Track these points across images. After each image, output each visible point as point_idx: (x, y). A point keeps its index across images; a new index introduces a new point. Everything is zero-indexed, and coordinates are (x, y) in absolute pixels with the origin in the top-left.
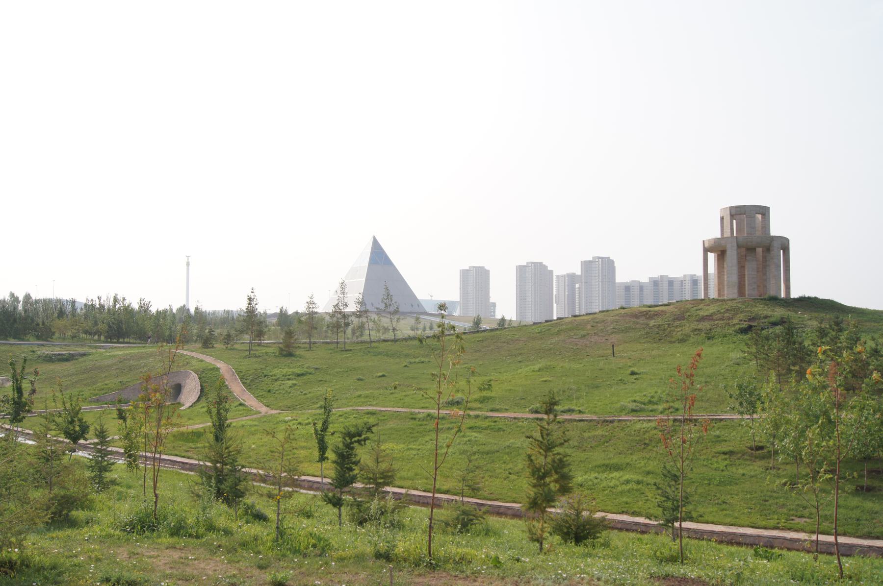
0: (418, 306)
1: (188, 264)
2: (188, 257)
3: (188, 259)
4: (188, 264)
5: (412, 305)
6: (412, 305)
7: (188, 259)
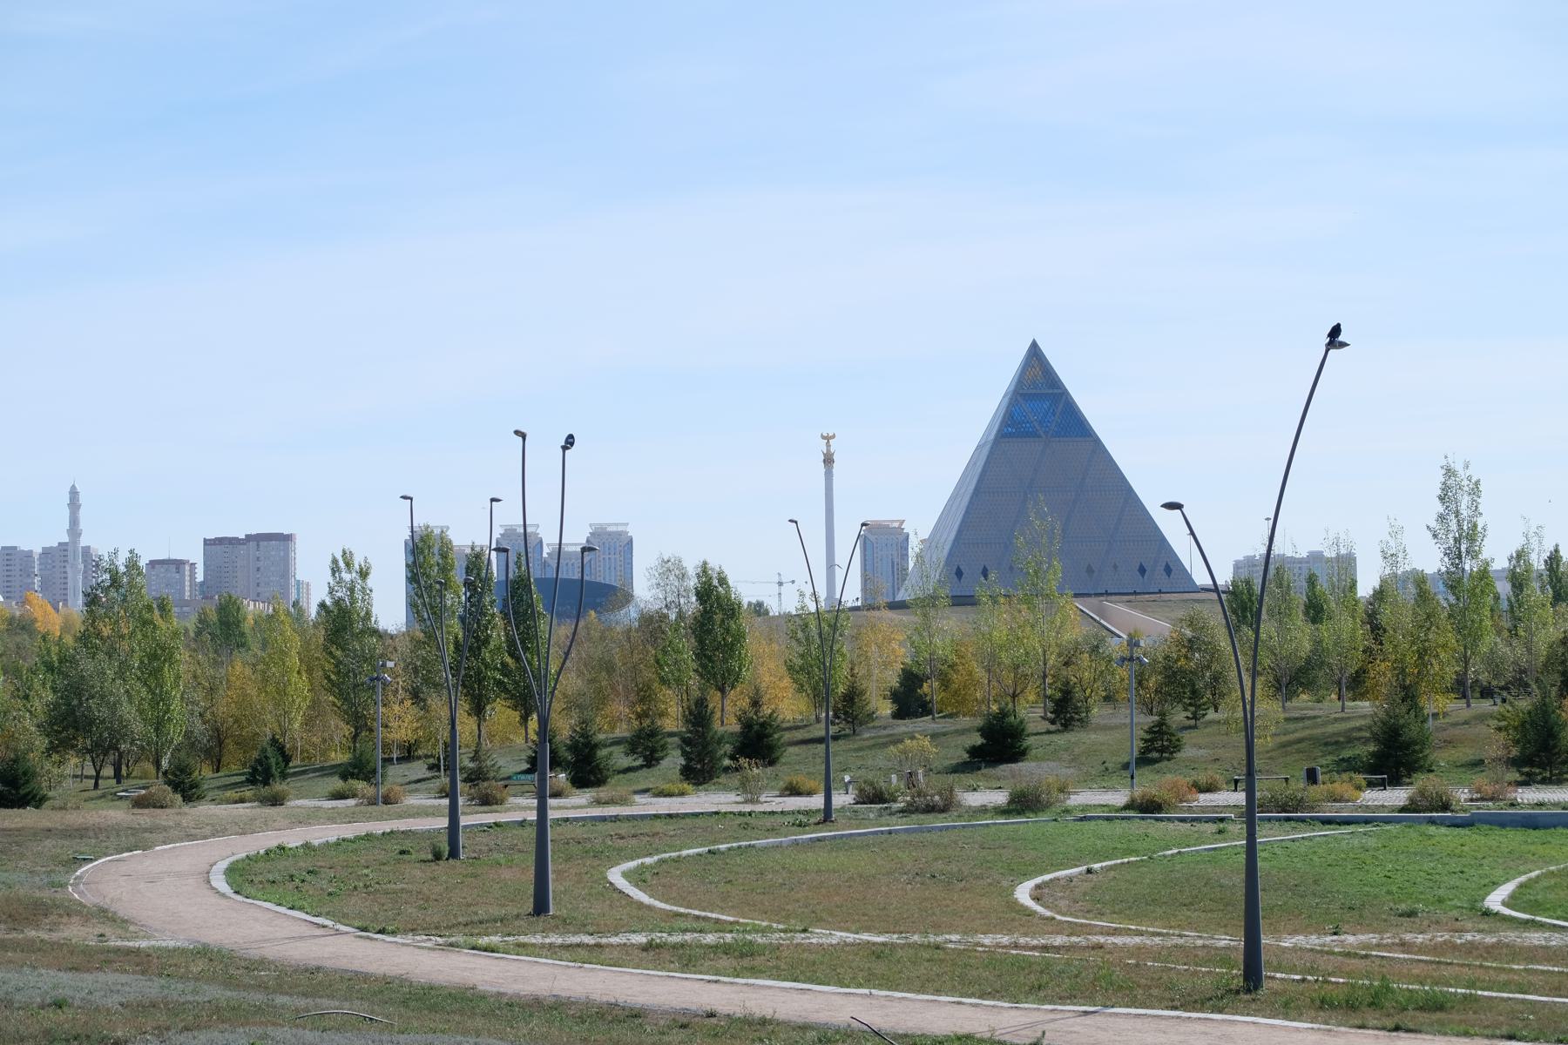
0: (1168, 570)
1: (828, 460)
2: (828, 438)
3: (828, 445)
4: (828, 460)
5: (1142, 570)
6: (1142, 570)
7: (828, 445)
